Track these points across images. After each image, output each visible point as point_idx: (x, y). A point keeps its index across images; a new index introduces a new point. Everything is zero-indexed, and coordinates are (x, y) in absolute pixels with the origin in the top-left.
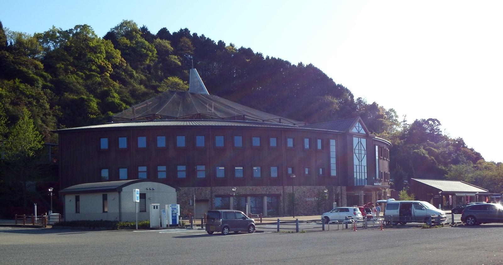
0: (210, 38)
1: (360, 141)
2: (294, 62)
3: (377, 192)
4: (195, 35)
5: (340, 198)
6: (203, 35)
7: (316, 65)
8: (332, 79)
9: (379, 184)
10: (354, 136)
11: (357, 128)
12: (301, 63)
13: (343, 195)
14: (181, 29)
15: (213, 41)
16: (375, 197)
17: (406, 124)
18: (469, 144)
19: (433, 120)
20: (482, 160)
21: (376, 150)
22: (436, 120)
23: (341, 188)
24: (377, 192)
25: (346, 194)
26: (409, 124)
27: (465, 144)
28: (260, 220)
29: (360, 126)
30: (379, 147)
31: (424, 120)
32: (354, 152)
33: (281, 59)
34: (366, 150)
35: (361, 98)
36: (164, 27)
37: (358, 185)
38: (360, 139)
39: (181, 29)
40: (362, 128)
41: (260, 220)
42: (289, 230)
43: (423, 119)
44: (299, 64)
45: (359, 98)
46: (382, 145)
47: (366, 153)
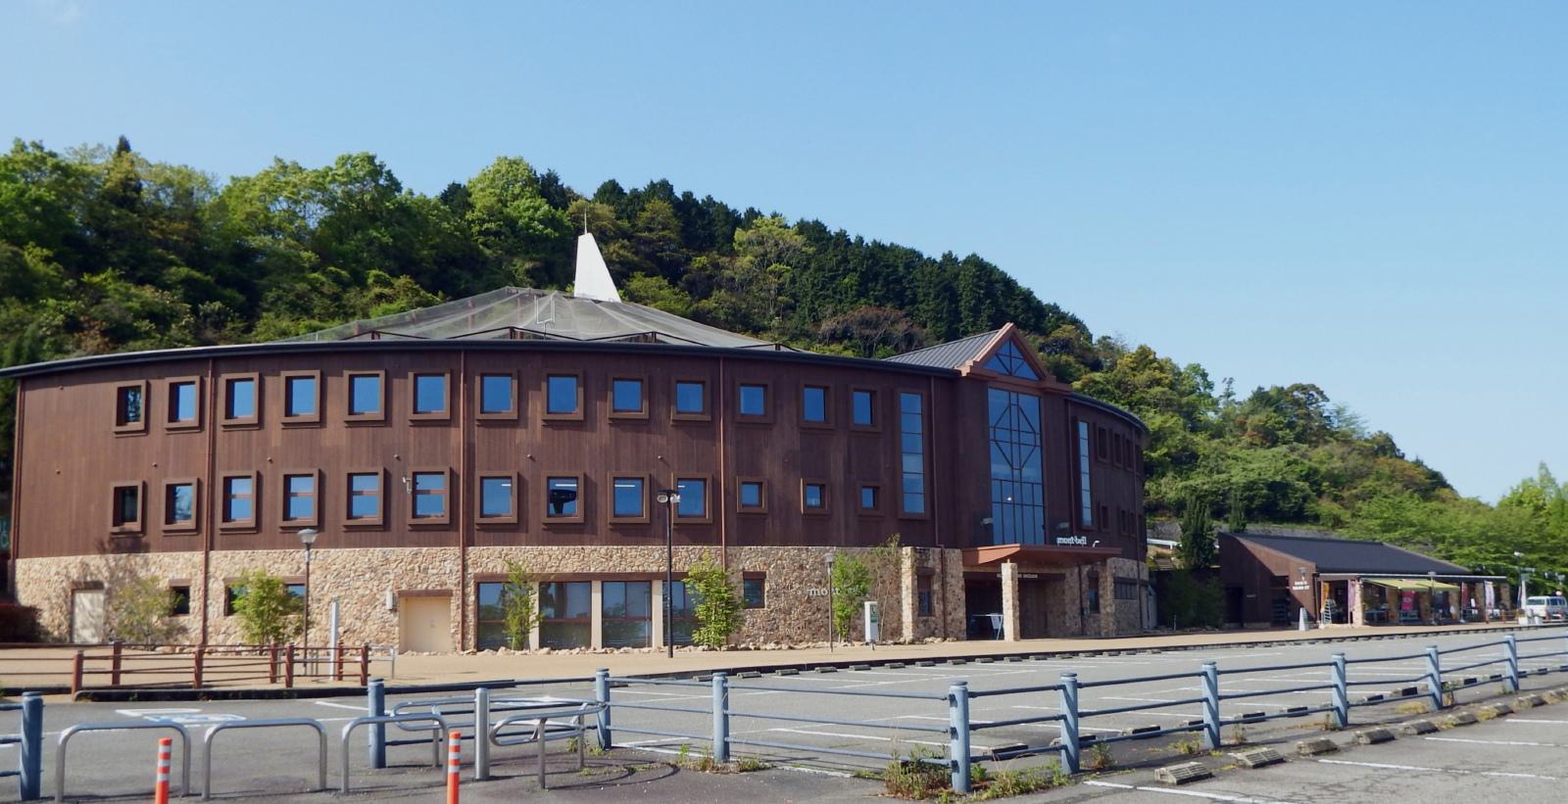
0: (724, 203)
1: (1014, 401)
2: (933, 251)
3: (1086, 569)
4: (688, 195)
5: (936, 587)
6: (709, 198)
7: (989, 257)
8: (1032, 293)
9: (1079, 541)
10: (990, 384)
11: (1006, 360)
12: (950, 253)
13: (949, 579)
14: (652, 182)
15: (735, 210)
16: (1077, 585)
17: (1233, 400)
18: (1410, 448)
19: (1303, 388)
20: (1447, 490)
21: (1081, 436)
22: (1313, 387)
23: (942, 553)
24: (1086, 569)
25: (961, 575)
26: (1241, 400)
27: (1399, 450)
28: (305, 657)
29: (1016, 353)
30: (1092, 429)
31: (1280, 390)
32: (992, 437)
33: (897, 247)
34: (1037, 430)
35: (1109, 338)
36: (611, 178)
37: (378, 383)
38: (1013, 395)
39: (652, 182)
40: (1021, 361)
41: (305, 657)
42: (1376, 691)
43: (1280, 385)
44: (944, 256)
45: (1104, 338)
46: (1104, 423)
47: (1038, 443)
